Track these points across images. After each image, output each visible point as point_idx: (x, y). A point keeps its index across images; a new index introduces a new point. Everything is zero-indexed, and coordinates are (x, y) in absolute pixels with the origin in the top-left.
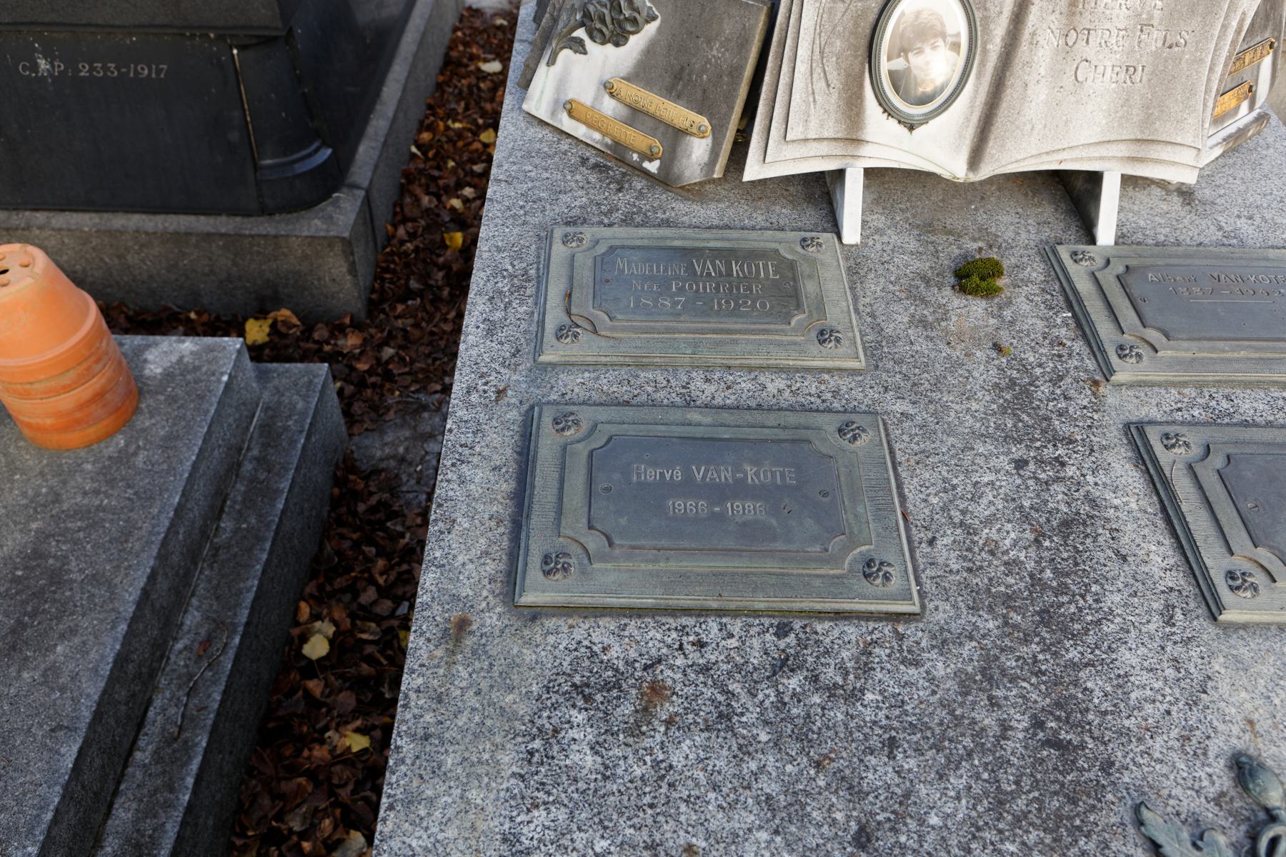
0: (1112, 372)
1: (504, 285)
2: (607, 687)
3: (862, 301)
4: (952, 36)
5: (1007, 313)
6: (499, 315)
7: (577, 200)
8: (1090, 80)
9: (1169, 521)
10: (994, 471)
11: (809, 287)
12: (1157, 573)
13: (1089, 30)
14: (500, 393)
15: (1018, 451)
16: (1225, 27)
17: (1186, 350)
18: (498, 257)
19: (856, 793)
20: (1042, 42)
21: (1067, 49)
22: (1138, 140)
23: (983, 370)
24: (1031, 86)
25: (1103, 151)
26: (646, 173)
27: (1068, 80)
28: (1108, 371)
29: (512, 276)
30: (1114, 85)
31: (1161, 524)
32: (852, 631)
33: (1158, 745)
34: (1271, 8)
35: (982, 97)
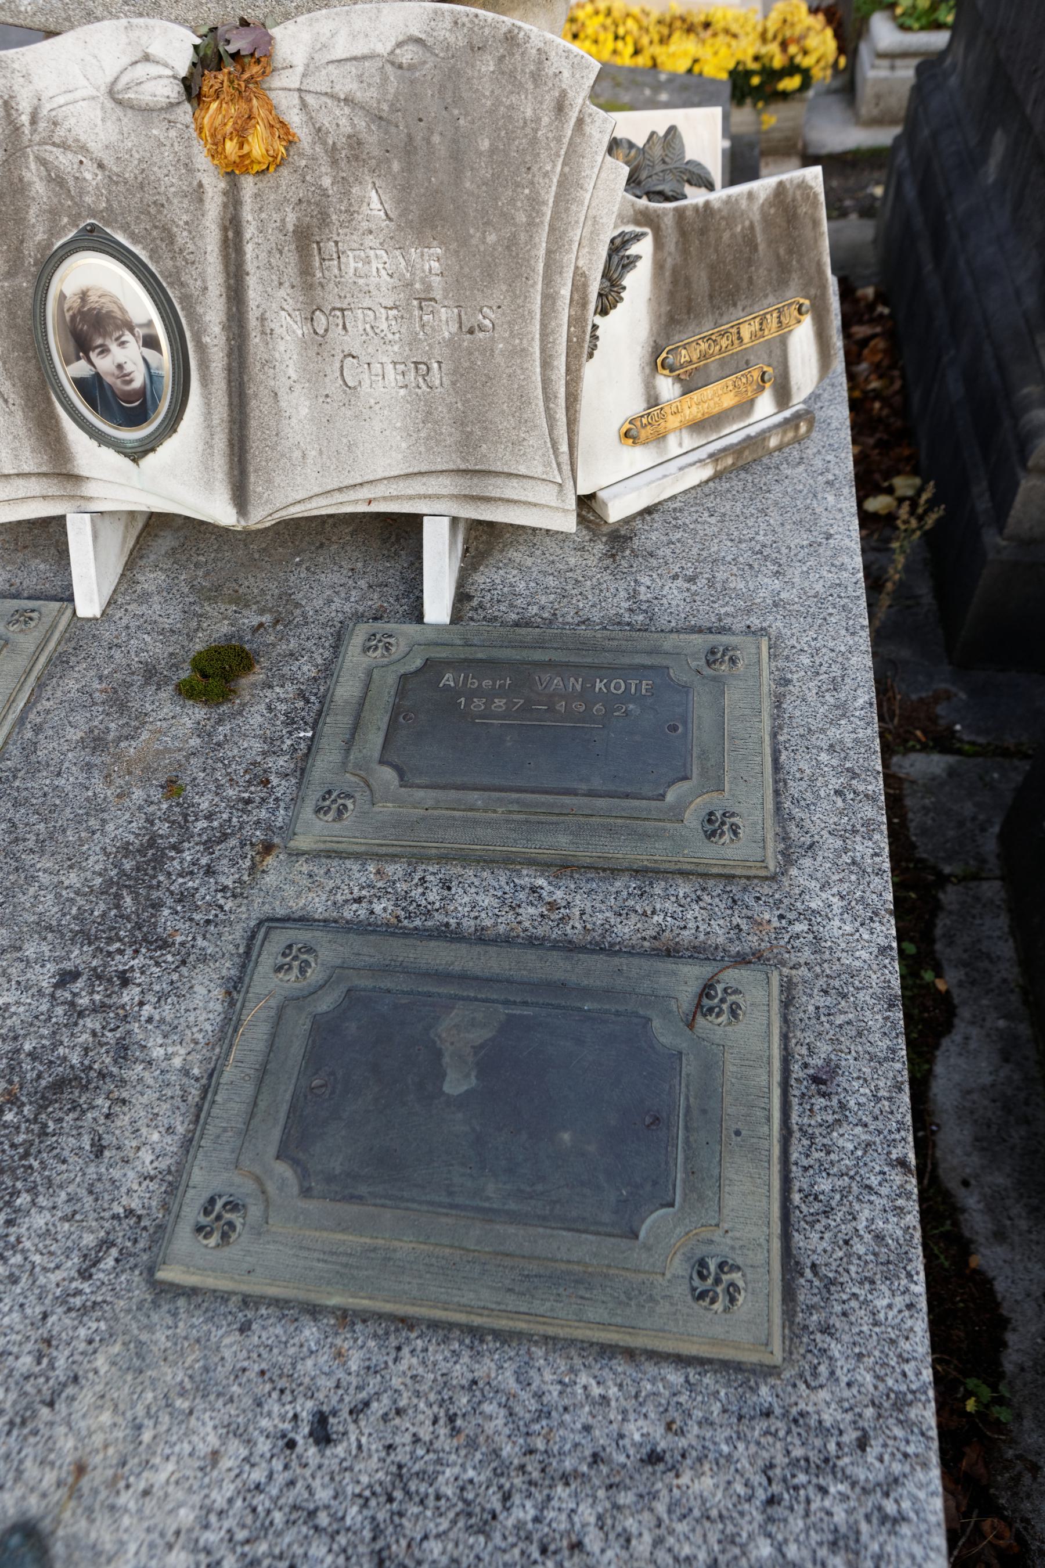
4: (141, 326)
8: (366, 384)
13: (342, 310)
16: (549, 298)
20: (278, 331)
21: (317, 343)
22: (466, 472)
24: (282, 393)
25: (417, 487)
27: (333, 386)
30: (402, 392)
34: (790, 252)
35: (221, 411)
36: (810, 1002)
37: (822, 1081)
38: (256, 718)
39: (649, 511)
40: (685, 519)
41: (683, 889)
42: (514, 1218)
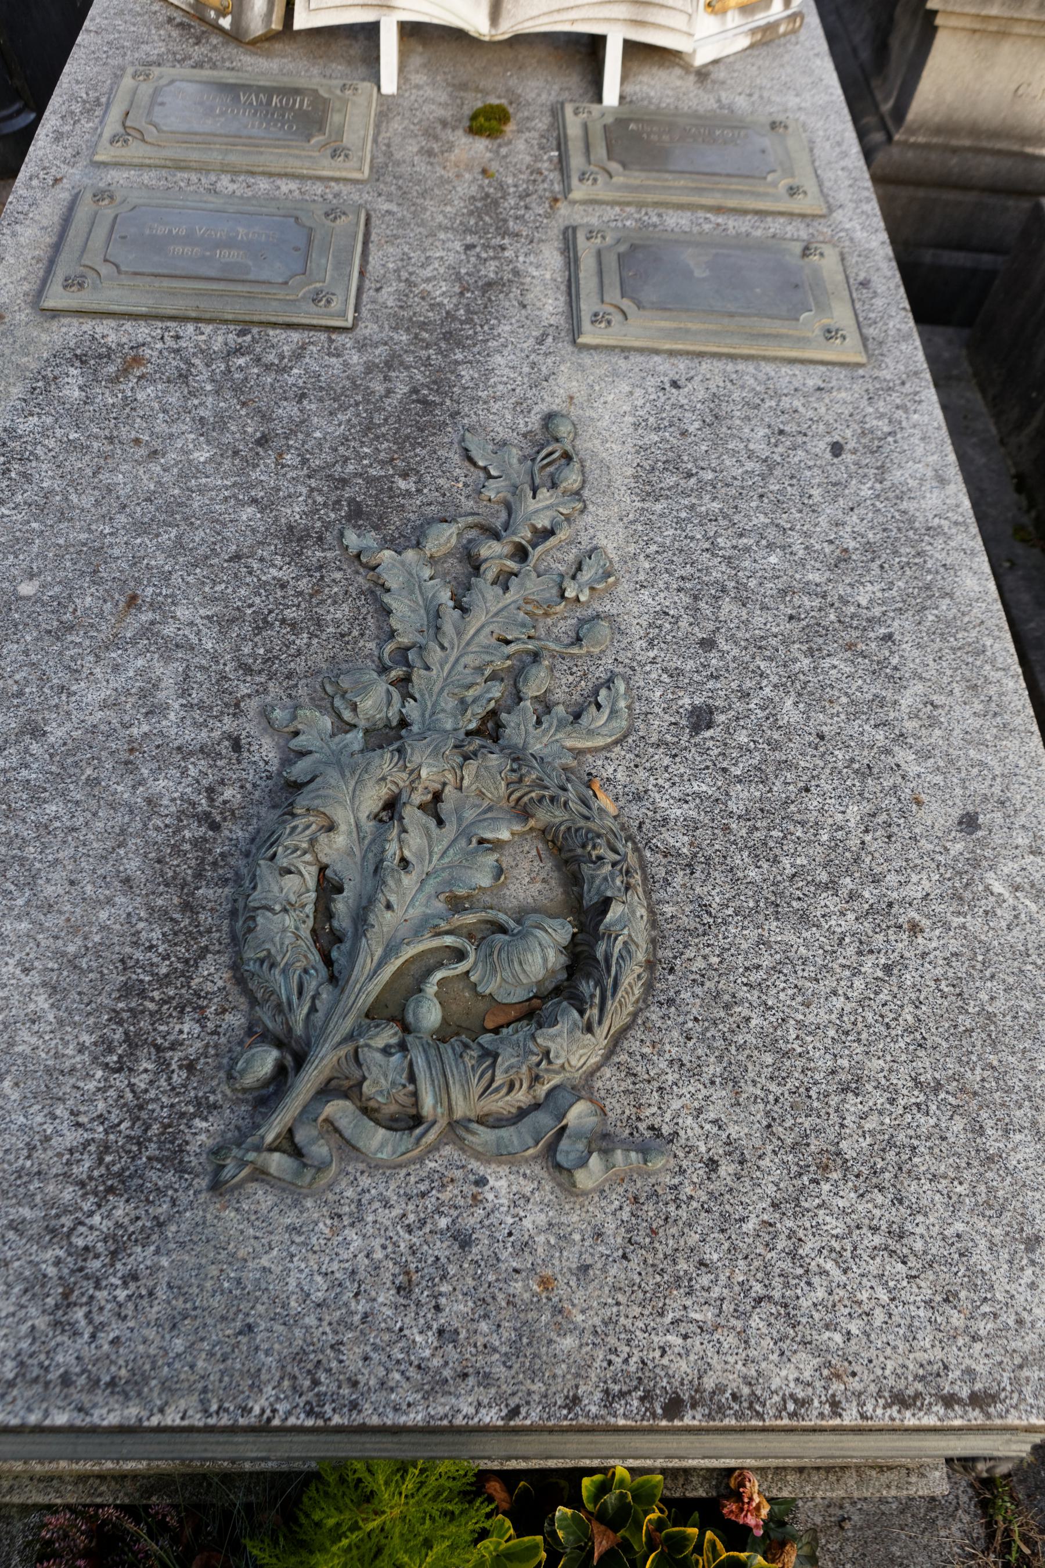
0: (570, 190)
1: (77, 108)
2: (100, 356)
3: (383, 135)
5: (504, 151)
6: (67, 128)
7: (156, 49)
9: (569, 287)
10: (448, 250)
11: (336, 118)
12: (545, 314)
14: (56, 181)
15: (469, 239)
17: (637, 178)
18: (76, 87)
19: (265, 417)
23: (467, 187)
26: (221, 29)
28: (567, 190)
29: (84, 102)
31: (563, 288)
32: (295, 336)
33: (495, 407)
36: (853, 260)
37: (865, 284)
38: (520, 145)
39: (715, 62)
40: (737, 66)
41: (782, 220)
42: (743, 315)
